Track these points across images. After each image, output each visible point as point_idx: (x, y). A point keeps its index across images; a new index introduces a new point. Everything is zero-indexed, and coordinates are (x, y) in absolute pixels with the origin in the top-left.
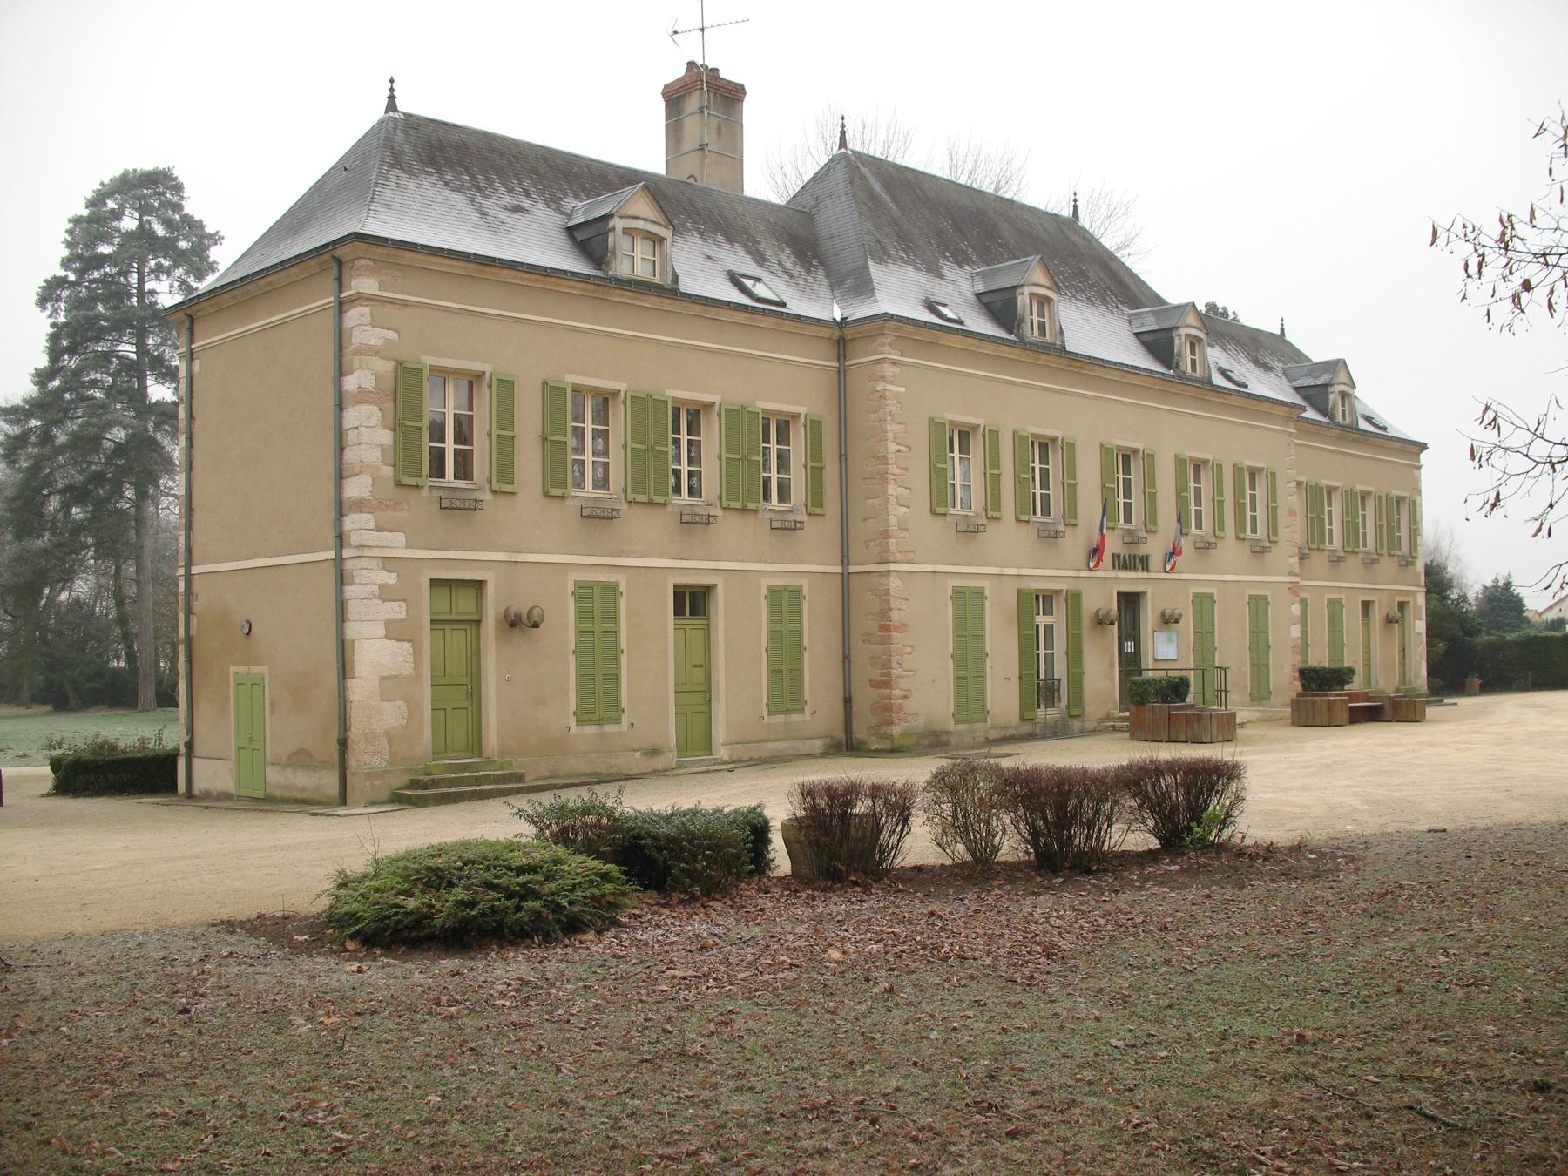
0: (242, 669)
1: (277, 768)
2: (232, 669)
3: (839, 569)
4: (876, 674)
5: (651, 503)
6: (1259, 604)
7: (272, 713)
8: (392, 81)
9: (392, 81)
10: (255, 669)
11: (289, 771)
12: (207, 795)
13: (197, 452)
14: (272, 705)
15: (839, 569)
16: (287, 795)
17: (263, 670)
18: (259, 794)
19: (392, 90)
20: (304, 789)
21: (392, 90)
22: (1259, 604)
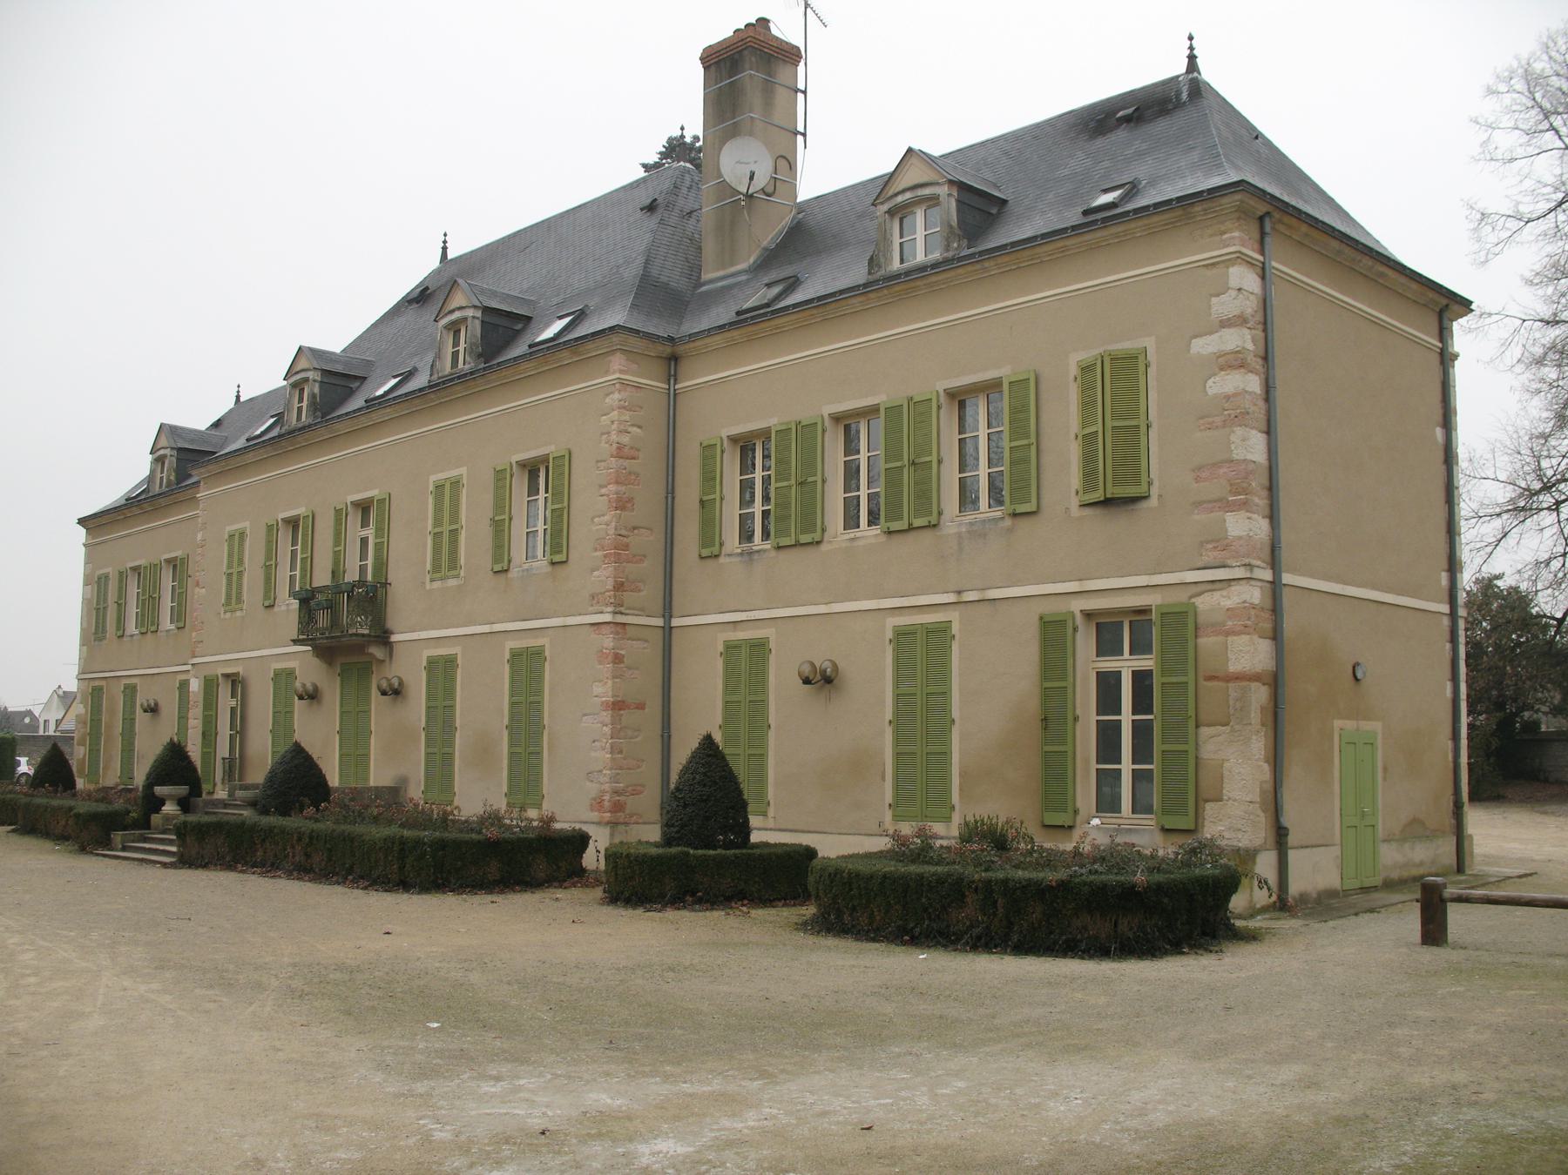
0: (1349, 725)
1: (1394, 845)
2: (1338, 723)
3: (659, 622)
4: (628, 717)
5: (798, 544)
6: (527, 667)
7: (1385, 779)
8: (1191, 38)
9: (1191, 38)
10: (1367, 726)
11: (1407, 845)
12: (1303, 899)
13: (1280, 394)
14: (1385, 769)
15: (659, 622)
16: (1405, 874)
17: (1376, 726)
18: (1377, 881)
19: (1191, 48)
20: (1421, 864)
21: (1191, 48)
22: (527, 667)
